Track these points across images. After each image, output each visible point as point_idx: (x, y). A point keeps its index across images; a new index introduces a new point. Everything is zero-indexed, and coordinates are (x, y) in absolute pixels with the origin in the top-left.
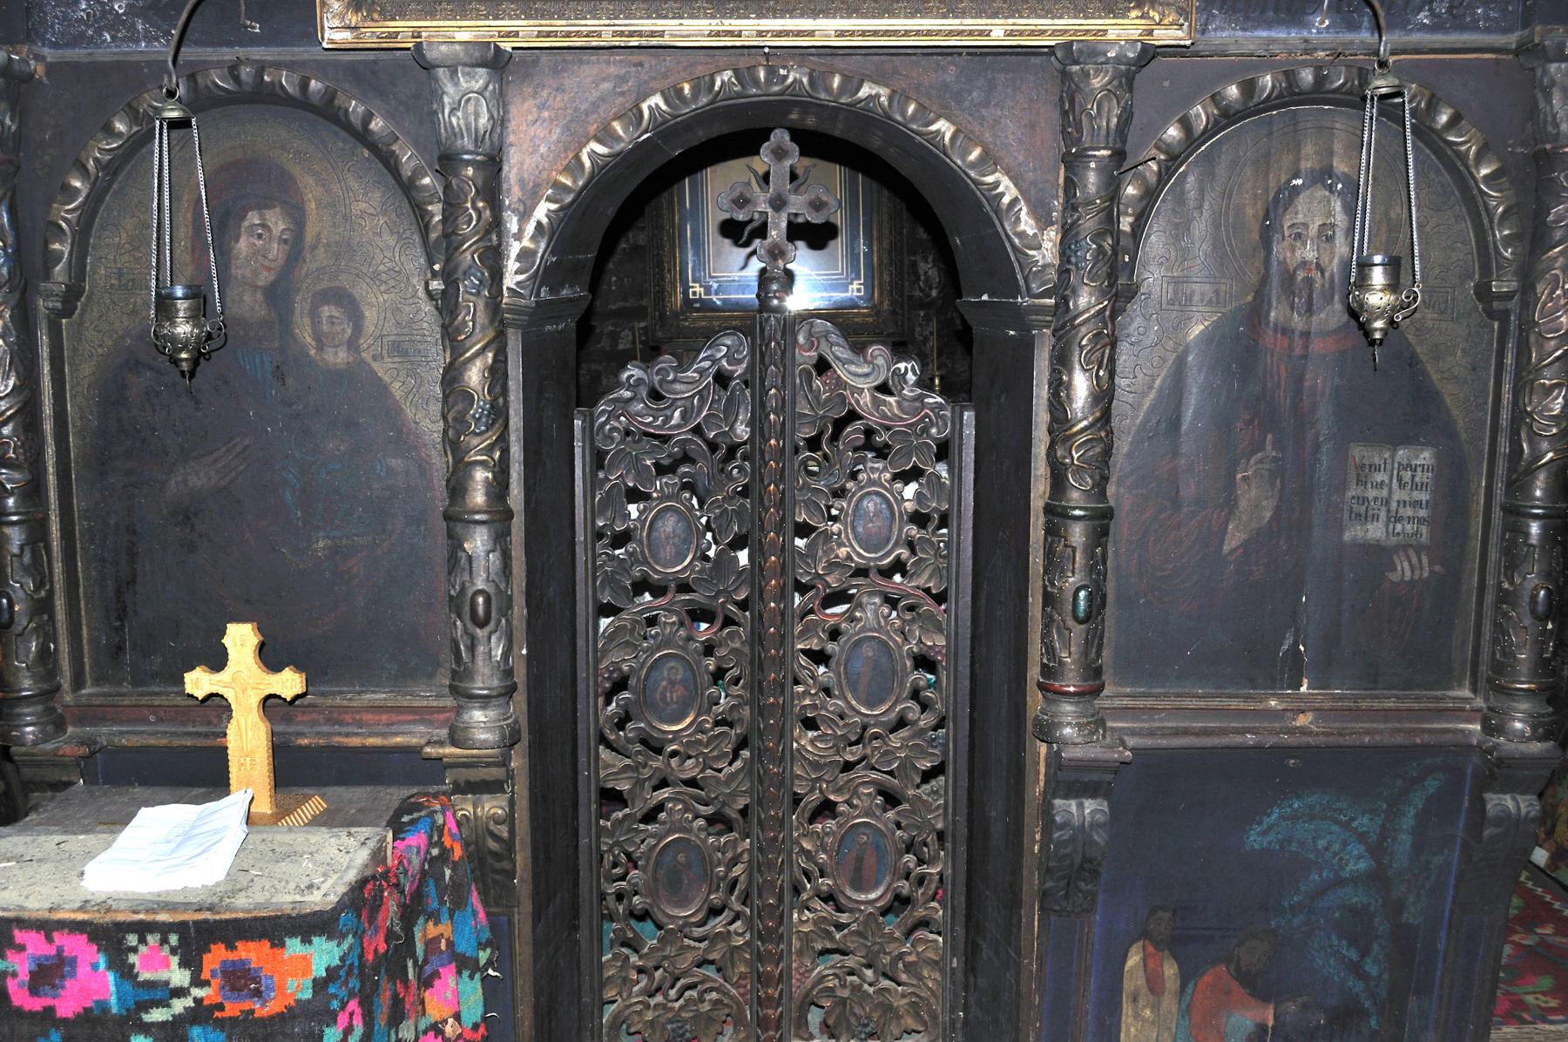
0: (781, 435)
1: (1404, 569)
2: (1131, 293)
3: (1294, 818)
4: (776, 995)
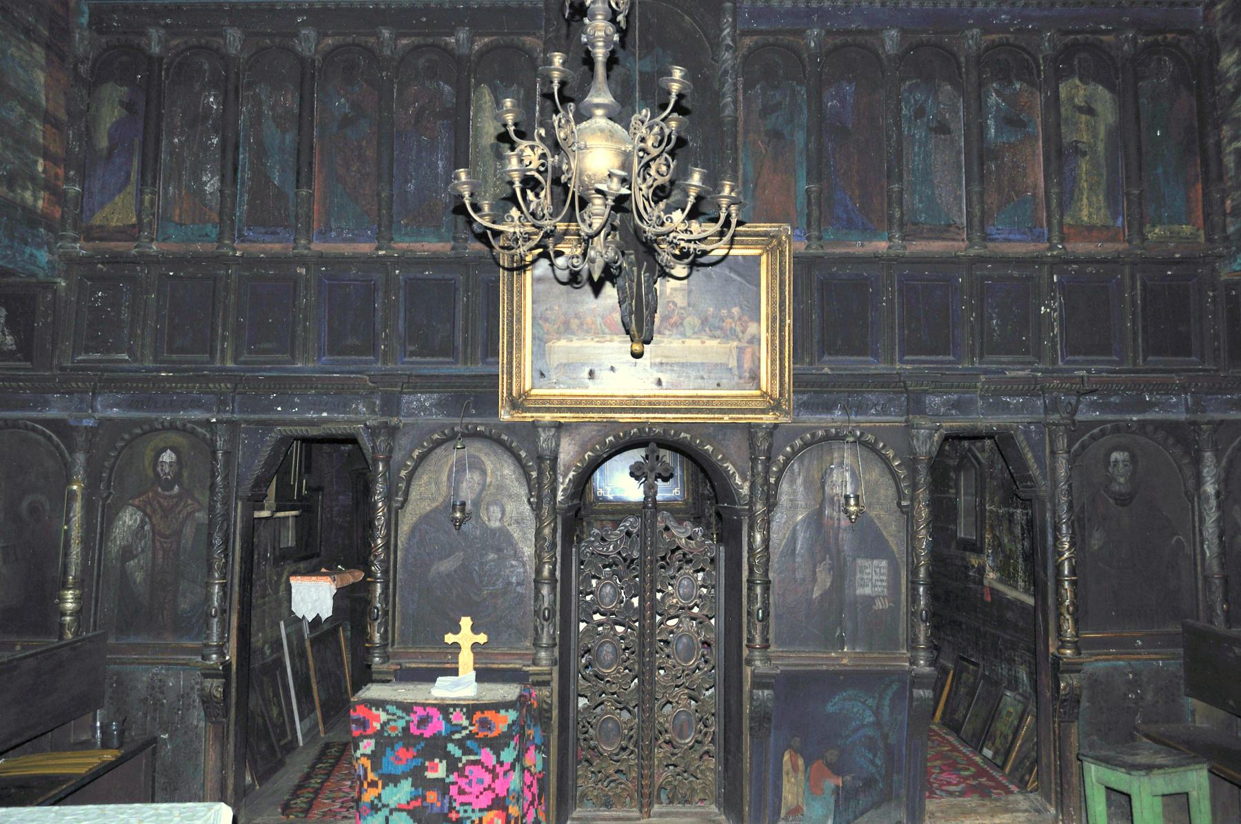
0: (652, 555)
1: (879, 605)
2: (775, 504)
3: (844, 700)
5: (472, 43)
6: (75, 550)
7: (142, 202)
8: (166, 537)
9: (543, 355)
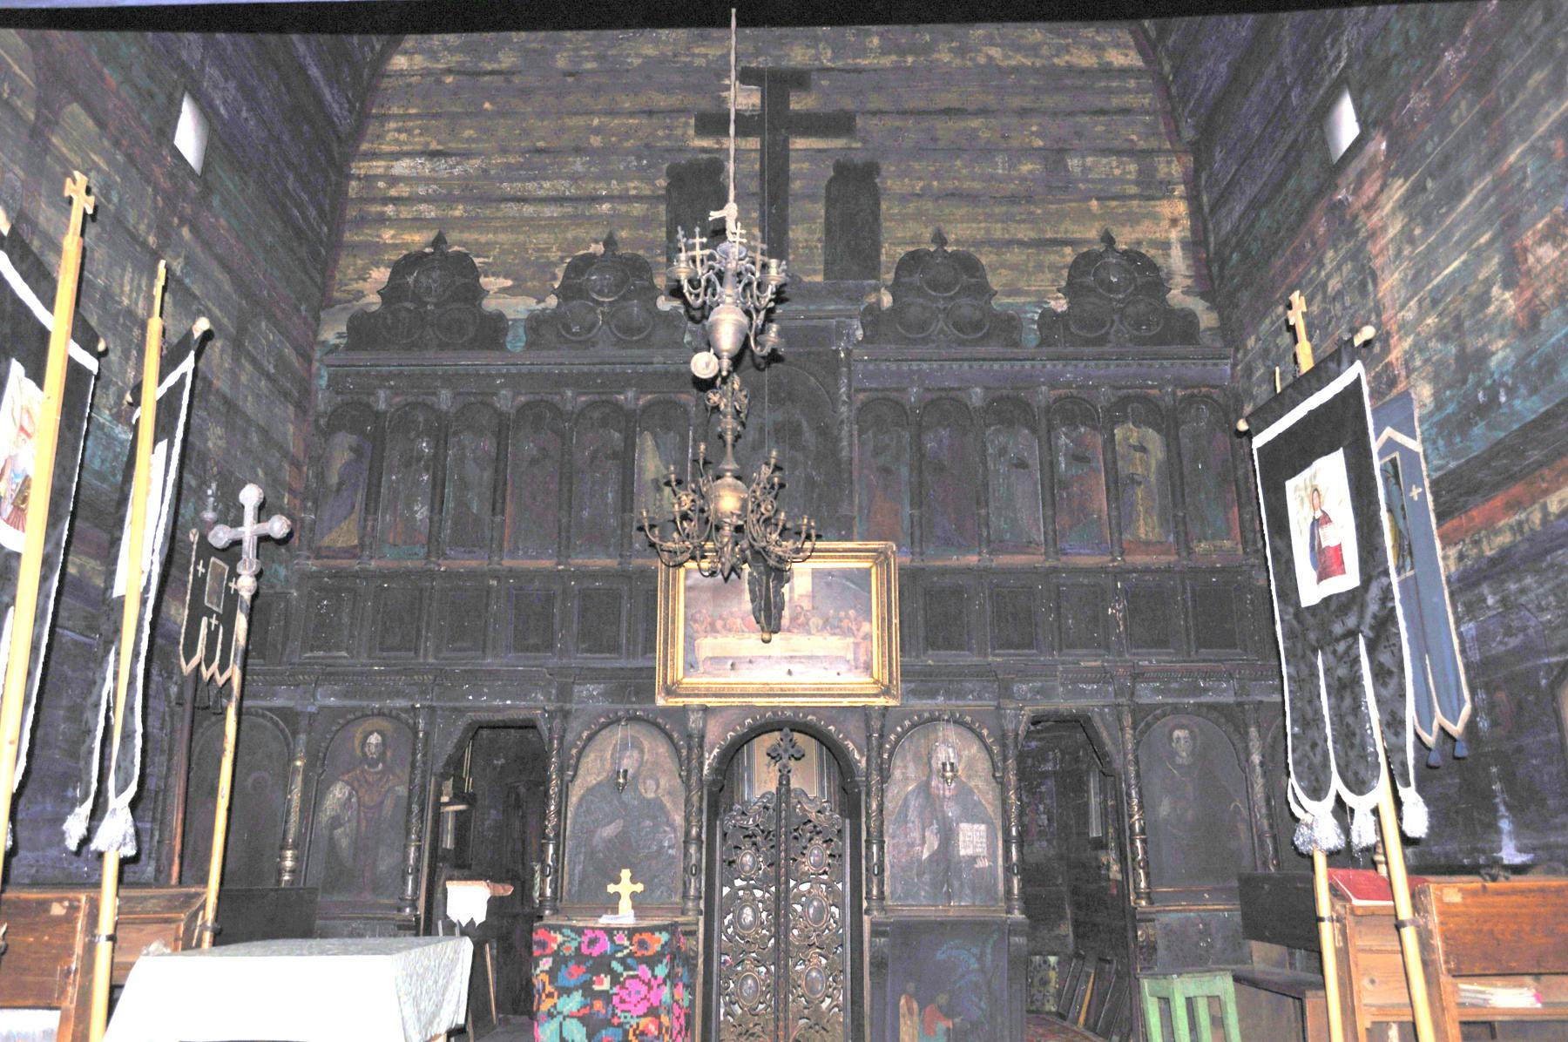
2: (889, 777)
5: (638, 399)
6: (294, 817)
7: (365, 528)
8: (371, 808)
9: (693, 650)
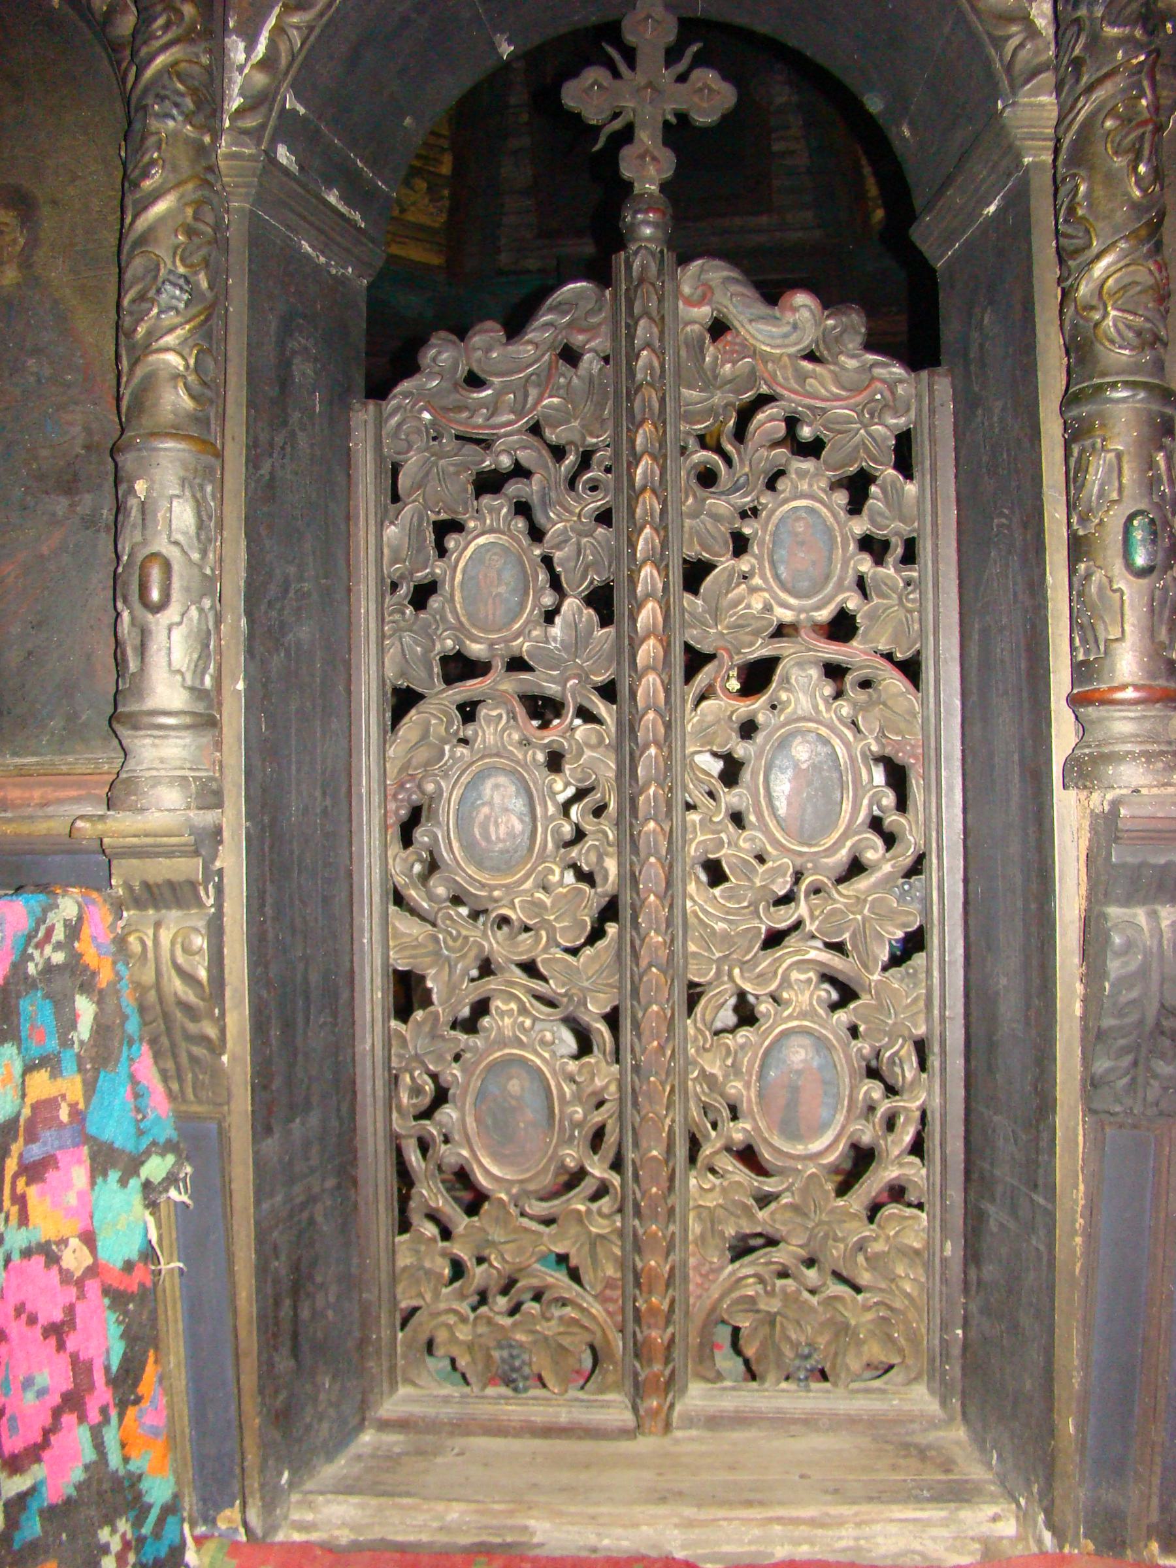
4: (665, 1306)
